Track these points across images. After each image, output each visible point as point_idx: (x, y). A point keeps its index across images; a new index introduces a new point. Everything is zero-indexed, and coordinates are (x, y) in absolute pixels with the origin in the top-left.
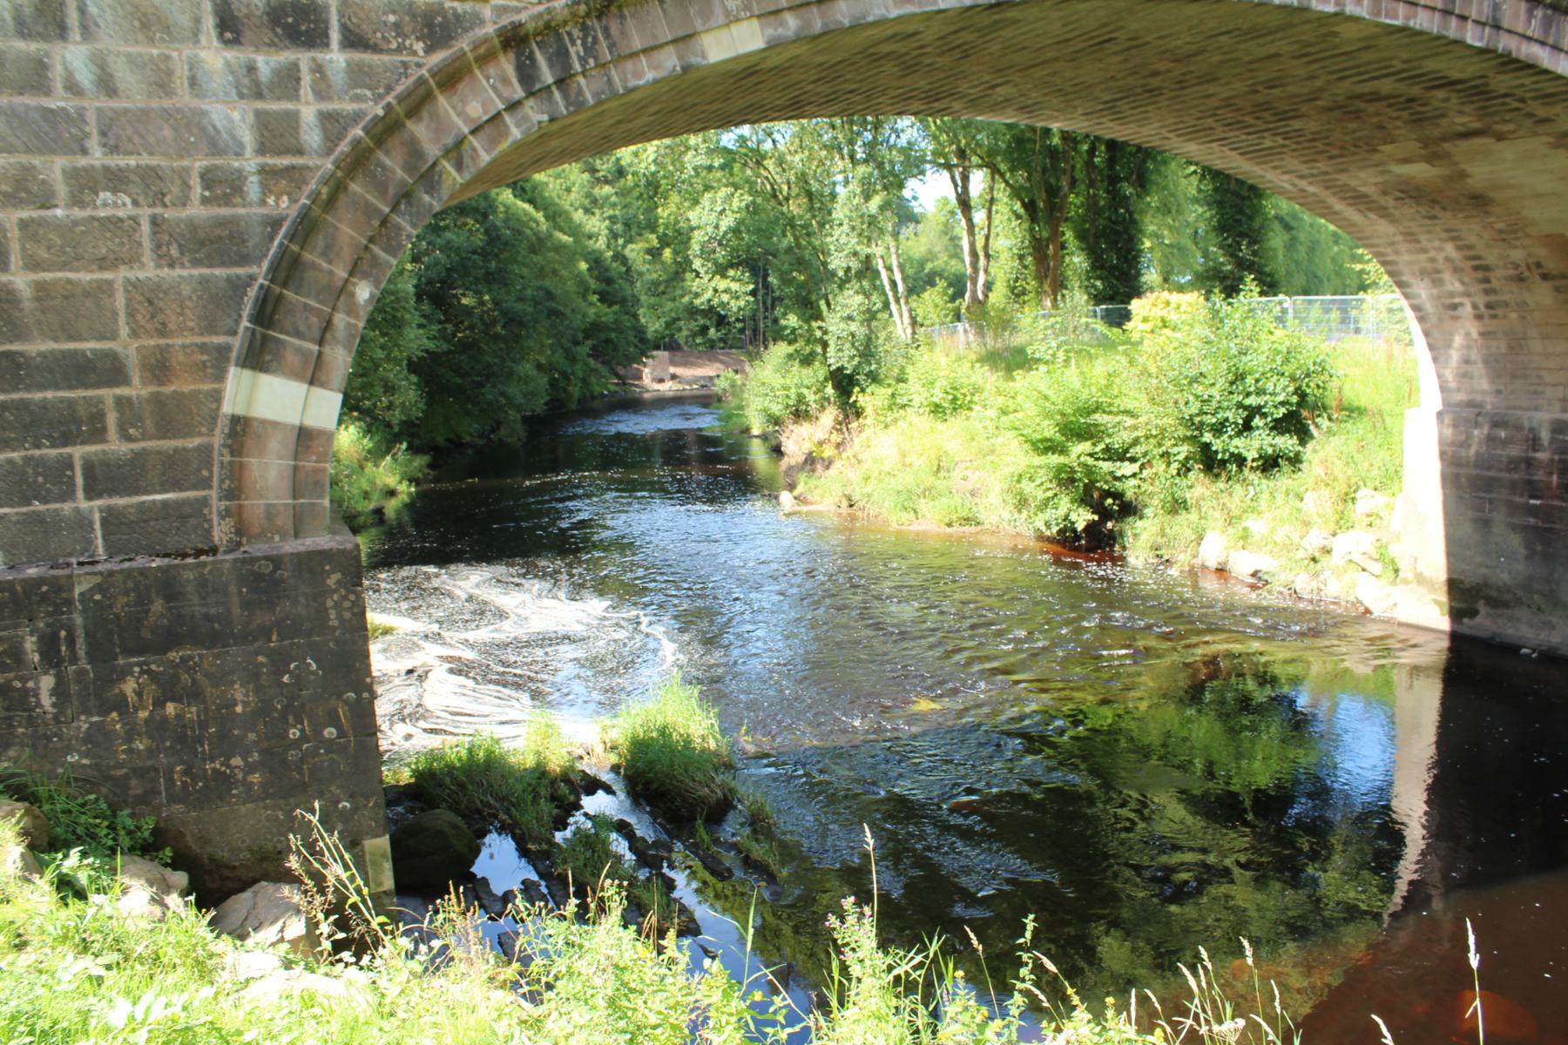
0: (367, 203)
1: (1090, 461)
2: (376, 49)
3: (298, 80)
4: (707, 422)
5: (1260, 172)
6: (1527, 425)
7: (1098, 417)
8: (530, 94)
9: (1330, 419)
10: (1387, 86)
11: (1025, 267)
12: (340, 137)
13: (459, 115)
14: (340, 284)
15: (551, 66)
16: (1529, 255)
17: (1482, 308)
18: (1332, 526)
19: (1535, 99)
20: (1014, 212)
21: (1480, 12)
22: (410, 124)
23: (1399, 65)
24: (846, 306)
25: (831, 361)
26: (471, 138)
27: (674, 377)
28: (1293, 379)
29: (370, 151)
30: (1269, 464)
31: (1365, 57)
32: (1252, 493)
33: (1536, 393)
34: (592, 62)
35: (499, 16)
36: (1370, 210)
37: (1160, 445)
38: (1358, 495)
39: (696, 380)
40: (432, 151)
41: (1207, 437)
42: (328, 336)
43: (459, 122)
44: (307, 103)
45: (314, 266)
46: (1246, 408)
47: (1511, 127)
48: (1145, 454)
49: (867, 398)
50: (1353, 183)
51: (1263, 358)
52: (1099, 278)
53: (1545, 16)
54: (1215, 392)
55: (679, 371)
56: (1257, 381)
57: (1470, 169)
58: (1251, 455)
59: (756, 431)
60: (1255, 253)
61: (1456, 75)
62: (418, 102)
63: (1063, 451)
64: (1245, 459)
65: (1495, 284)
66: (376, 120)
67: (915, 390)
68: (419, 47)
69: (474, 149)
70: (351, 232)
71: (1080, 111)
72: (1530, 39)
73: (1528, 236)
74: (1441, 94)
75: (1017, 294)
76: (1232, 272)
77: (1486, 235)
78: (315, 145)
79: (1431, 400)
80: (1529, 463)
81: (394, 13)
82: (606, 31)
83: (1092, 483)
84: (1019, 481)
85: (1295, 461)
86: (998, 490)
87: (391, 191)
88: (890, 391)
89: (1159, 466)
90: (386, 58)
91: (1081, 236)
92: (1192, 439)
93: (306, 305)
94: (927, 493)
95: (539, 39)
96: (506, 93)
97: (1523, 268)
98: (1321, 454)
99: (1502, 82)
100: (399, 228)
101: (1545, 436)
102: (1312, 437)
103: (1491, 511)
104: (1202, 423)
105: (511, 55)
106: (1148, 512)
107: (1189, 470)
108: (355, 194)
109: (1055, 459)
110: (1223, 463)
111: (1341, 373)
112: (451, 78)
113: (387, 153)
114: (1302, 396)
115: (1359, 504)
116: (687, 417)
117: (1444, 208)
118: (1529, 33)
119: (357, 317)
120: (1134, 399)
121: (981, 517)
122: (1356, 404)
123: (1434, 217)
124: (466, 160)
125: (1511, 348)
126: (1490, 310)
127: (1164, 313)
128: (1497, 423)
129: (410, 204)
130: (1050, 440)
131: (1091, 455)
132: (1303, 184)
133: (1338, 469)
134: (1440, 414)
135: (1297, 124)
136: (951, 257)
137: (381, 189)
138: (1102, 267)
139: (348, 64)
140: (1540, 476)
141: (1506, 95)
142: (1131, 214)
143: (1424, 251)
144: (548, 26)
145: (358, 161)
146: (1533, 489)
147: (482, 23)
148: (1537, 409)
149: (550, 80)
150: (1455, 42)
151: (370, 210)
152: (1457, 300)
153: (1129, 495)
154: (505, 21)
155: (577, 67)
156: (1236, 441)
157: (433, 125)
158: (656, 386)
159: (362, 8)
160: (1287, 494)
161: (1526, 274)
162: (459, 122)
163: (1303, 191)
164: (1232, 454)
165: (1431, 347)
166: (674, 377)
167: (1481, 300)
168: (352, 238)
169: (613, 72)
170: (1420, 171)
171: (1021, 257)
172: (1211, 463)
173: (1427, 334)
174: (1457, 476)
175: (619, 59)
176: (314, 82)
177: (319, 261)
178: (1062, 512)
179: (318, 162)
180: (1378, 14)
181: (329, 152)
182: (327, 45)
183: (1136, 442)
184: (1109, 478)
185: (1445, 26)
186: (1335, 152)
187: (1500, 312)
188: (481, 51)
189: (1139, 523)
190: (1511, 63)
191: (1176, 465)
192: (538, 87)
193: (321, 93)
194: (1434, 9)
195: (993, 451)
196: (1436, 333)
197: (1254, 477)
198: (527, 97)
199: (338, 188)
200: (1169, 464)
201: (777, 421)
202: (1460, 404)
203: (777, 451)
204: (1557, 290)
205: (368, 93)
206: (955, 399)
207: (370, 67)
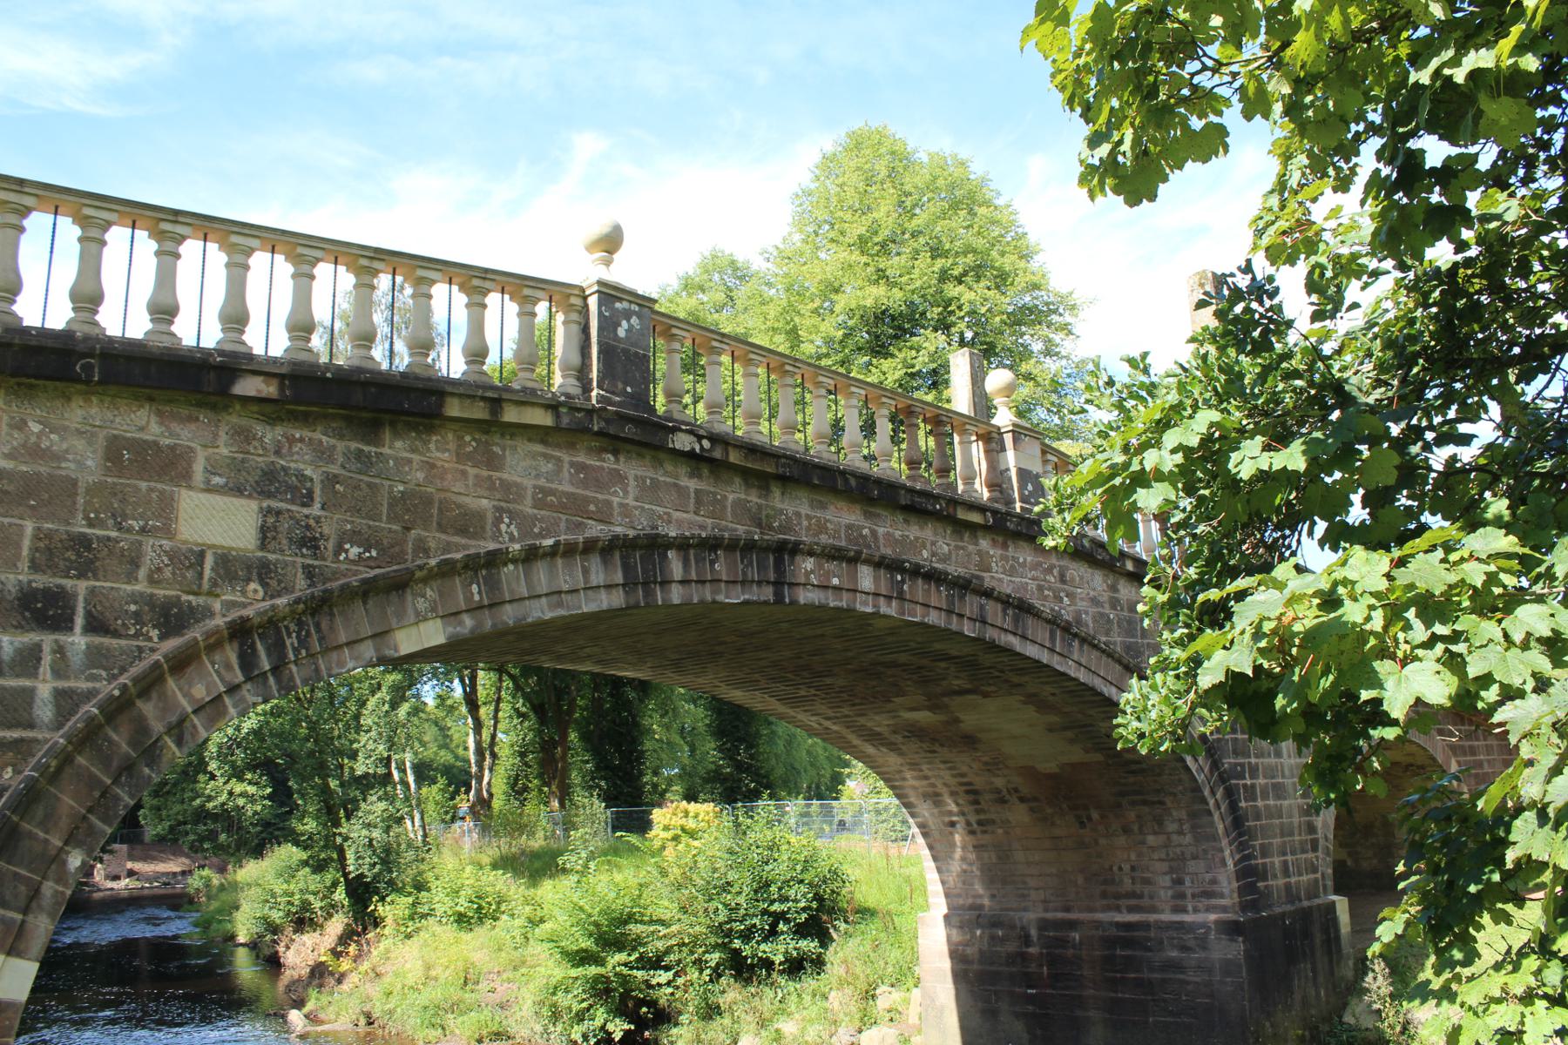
0: (92, 776)
1: (625, 971)
2: (116, 634)
3: (39, 659)
4: (178, 927)
5: (793, 714)
6: (1018, 924)
7: (635, 929)
8: (248, 679)
9: (846, 922)
10: (903, 658)
11: (526, 764)
12: (73, 712)
13: (184, 696)
14: (53, 852)
15: (269, 655)
16: (1009, 782)
17: (975, 826)
18: (858, 1024)
19: (1011, 671)
20: (517, 710)
21: (972, 612)
22: (139, 703)
23: (913, 645)
24: (369, 812)
25: (351, 868)
26: (192, 716)
27: (131, 873)
28: (811, 884)
29: (100, 726)
30: (795, 967)
31: (890, 639)
32: (780, 995)
33: (1023, 896)
34: (304, 652)
35: (228, 610)
36: (882, 744)
37: (692, 953)
38: (878, 992)
39: (157, 876)
40: (157, 727)
41: (737, 944)
42: (34, 905)
43: (184, 702)
44: (44, 681)
45: (31, 835)
46: (770, 914)
47: (992, 688)
48: (679, 961)
49: (388, 908)
50: (869, 724)
51: (784, 867)
52: (602, 778)
53: (1014, 614)
54: (741, 900)
55: (137, 866)
56: (780, 889)
57: (962, 716)
58: (778, 958)
59: (241, 939)
60: (752, 757)
61: (954, 653)
62: (150, 683)
63: (600, 962)
64: (773, 963)
65: (984, 805)
66: (111, 699)
67: (439, 899)
68: (154, 633)
69: (194, 727)
70: (72, 803)
71: (649, 665)
72: (1006, 630)
73: (1007, 767)
74: (943, 665)
75: (518, 790)
76: (731, 774)
77: (975, 765)
78: (46, 720)
79: (939, 906)
80: (1024, 957)
81: (136, 603)
82: (318, 626)
83: (628, 992)
84: (554, 994)
85: (819, 963)
86: (529, 1002)
87: (115, 764)
88: (410, 900)
89: (693, 974)
90: (123, 642)
91: (585, 737)
92: (723, 947)
93: (16, 874)
94: (455, 1007)
95: (260, 631)
96: (228, 677)
97: (1005, 792)
98: (841, 954)
99: (987, 659)
100: (117, 799)
101: (1034, 932)
102: (832, 940)
103: (996, 1001)
104: (731, 930)
105: (236, 645)
106: (684, 1018)
107: (720, 976)
108: (80, 766)
109: (593, 970)
110: (752, 966)
111: (852, 878)
112: (181, 663)
113: (115, 730)
114: (818, 898)
115: (879, 1002)
116: (153, 921)
117: (942, 745)
118: (1006, 626)
119: (66, 885)
120: (665, 908)
121: (512, 1031)
122: (866, 905)
123: (934, 752)
124: (187, 737)
125: (999, 858)
126: (980, 827)
127: (683, 821)
128: (995, 923)
129: (130, 776)
130: (586, 951)
131: (625, 965)
132: (827, 724)
133: (859, 969)
134: (946, 917)
135: (828, 681)
136: (440, 747)
137: (105, 762)
138: (607, 768)
139: (88, 646)
140: (1033, 968)
141: (990, 668)
142: (634, 717)
143: (926, 778)
144: (270, 621)
145: (89, 737)
146: (1029, 979)
147: (212, 615)
148: (1025, 909)
149: (267, 667)
150: (957, 633)
151: (93, 782)
152: (955, 819)
153: (663, 1002)
154: (234, 615)
155: (291, 656)
156: (763, 947)
157: (161, 705)
158: (110, 884)
159: (108, 599)
160: (814, 995)
161: (1007, 797)
162: (184, 702)
163: (827, 728)
164: (760, 959)
165: (935, 859)
166: (131, 873)
167: (973, 819)
168: (72, 808)
169: (320, 661)
170: (924, 717)
171: (522, 755)
172: (744, 969)
173: (931, 848)
174: (966, 972)
175: (327, 650)
176: (54, 661)
177: (35, 830)
178: (598, 1022)
179: (48, 736)
180: (904, 614)
181: (60, 726)
182: (71, 629)
183: (668, 951)
184: (643, 987)
185: (949, 622)
186: (857, 701)
187: (989, 828)
188: (212, 640)
189: (674, 1031)
190: (993, 647)
191: (708, 971)
192: (256, 673)
193: (58, 673)
194: (941, 609)
195: (524, 963)
196: (937, 846)
197: (782, 980)
198: (245, 682)
199: (66, 759)
200: (701, 971)
201: (275, 929)
202: (962, 908)
203: (273, 963)
204: (1031, 810)
205: (104, 674)
206: (480, 908)
207: (108, 649)
